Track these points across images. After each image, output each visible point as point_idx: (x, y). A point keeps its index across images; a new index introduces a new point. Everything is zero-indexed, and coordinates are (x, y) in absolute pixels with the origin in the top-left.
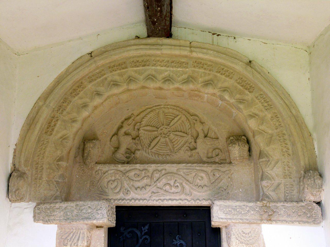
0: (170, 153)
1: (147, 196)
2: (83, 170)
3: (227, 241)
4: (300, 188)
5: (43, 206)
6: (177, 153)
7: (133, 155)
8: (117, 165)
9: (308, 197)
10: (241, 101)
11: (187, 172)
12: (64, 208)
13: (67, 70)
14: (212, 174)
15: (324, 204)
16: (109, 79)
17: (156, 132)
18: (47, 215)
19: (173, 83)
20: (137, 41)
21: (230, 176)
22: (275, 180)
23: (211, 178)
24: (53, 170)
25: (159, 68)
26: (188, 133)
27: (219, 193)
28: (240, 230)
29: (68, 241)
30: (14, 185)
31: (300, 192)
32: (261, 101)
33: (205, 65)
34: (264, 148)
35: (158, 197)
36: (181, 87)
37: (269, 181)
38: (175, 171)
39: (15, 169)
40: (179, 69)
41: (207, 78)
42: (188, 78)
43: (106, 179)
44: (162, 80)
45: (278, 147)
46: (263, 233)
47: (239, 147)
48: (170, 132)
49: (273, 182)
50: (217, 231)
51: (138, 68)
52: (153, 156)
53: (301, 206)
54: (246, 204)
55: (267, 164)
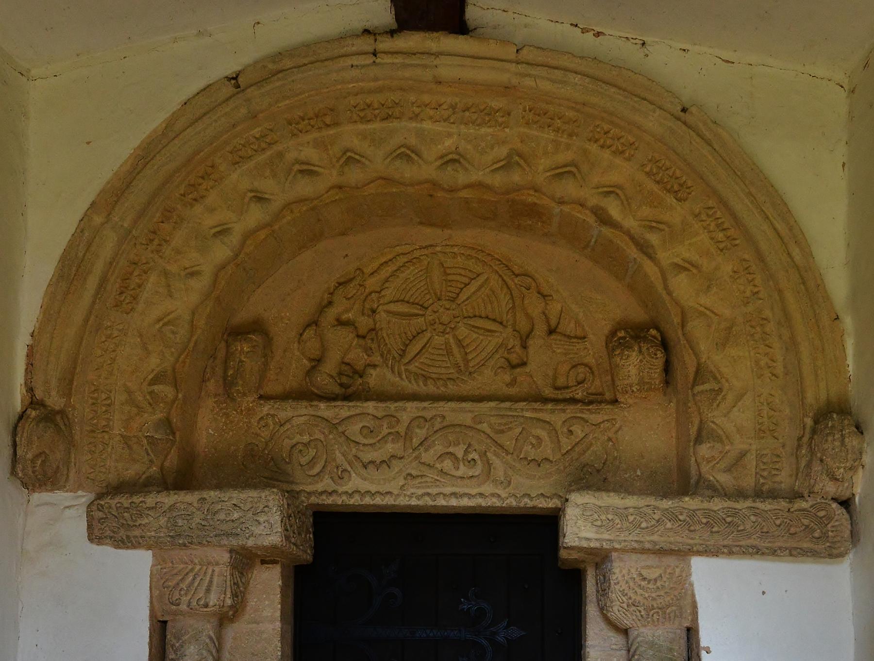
0: (456, 375)
1: (393, 487)
2: (227, 415)
3: (598, 601)
4: (798, 463)
5: (113, 502)
6: (475, 375)
7: (360, 381)
8: (315, 403)
9: (821, 485)
10: (653, 225)
11: (500, 424)
12: (167, 506)
13: (170, 124)
14: (565, 430)
15: (860, 504)
16: (291, 156)
17: (421, 320)
18: (123, 524)
19: (466, 169)
20: (366, 44)
21: (610, 435)
22: (732, 444)
23: (564, 440)
24: (138, 407)
25: (427, 125)
26: (505, 322)
27: (582, 479)
28: (633, 571)
29: (182, 593)
30: (30, 442)
31: (797, 474)
32: (709, 225)
33: (556, 118)
34: (709, 358)
35: (423, 488)
36: (488, 180)
37: (718, 445)
38: (469, 422)
39: (33, 402)
40: (484, 130)
41: (563, 157)
42: (509, 156)
43: (286, 440)
44: (436, 160)
45: (747, 354)
46: (694, 578)
47: (641, 357)
48: (458, 319)
49: (727, 448)
50: (574, 577)
51: (370, 126)
52: (410, 382)
53: (800, 510)
54: (654, 503)
55: (715, 399)
